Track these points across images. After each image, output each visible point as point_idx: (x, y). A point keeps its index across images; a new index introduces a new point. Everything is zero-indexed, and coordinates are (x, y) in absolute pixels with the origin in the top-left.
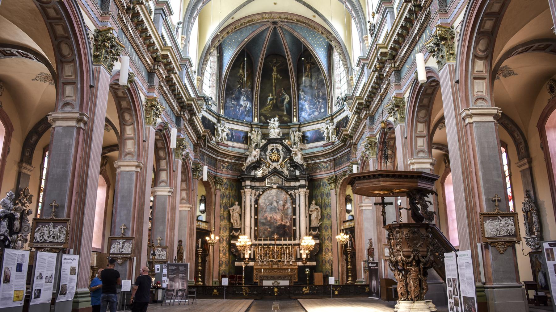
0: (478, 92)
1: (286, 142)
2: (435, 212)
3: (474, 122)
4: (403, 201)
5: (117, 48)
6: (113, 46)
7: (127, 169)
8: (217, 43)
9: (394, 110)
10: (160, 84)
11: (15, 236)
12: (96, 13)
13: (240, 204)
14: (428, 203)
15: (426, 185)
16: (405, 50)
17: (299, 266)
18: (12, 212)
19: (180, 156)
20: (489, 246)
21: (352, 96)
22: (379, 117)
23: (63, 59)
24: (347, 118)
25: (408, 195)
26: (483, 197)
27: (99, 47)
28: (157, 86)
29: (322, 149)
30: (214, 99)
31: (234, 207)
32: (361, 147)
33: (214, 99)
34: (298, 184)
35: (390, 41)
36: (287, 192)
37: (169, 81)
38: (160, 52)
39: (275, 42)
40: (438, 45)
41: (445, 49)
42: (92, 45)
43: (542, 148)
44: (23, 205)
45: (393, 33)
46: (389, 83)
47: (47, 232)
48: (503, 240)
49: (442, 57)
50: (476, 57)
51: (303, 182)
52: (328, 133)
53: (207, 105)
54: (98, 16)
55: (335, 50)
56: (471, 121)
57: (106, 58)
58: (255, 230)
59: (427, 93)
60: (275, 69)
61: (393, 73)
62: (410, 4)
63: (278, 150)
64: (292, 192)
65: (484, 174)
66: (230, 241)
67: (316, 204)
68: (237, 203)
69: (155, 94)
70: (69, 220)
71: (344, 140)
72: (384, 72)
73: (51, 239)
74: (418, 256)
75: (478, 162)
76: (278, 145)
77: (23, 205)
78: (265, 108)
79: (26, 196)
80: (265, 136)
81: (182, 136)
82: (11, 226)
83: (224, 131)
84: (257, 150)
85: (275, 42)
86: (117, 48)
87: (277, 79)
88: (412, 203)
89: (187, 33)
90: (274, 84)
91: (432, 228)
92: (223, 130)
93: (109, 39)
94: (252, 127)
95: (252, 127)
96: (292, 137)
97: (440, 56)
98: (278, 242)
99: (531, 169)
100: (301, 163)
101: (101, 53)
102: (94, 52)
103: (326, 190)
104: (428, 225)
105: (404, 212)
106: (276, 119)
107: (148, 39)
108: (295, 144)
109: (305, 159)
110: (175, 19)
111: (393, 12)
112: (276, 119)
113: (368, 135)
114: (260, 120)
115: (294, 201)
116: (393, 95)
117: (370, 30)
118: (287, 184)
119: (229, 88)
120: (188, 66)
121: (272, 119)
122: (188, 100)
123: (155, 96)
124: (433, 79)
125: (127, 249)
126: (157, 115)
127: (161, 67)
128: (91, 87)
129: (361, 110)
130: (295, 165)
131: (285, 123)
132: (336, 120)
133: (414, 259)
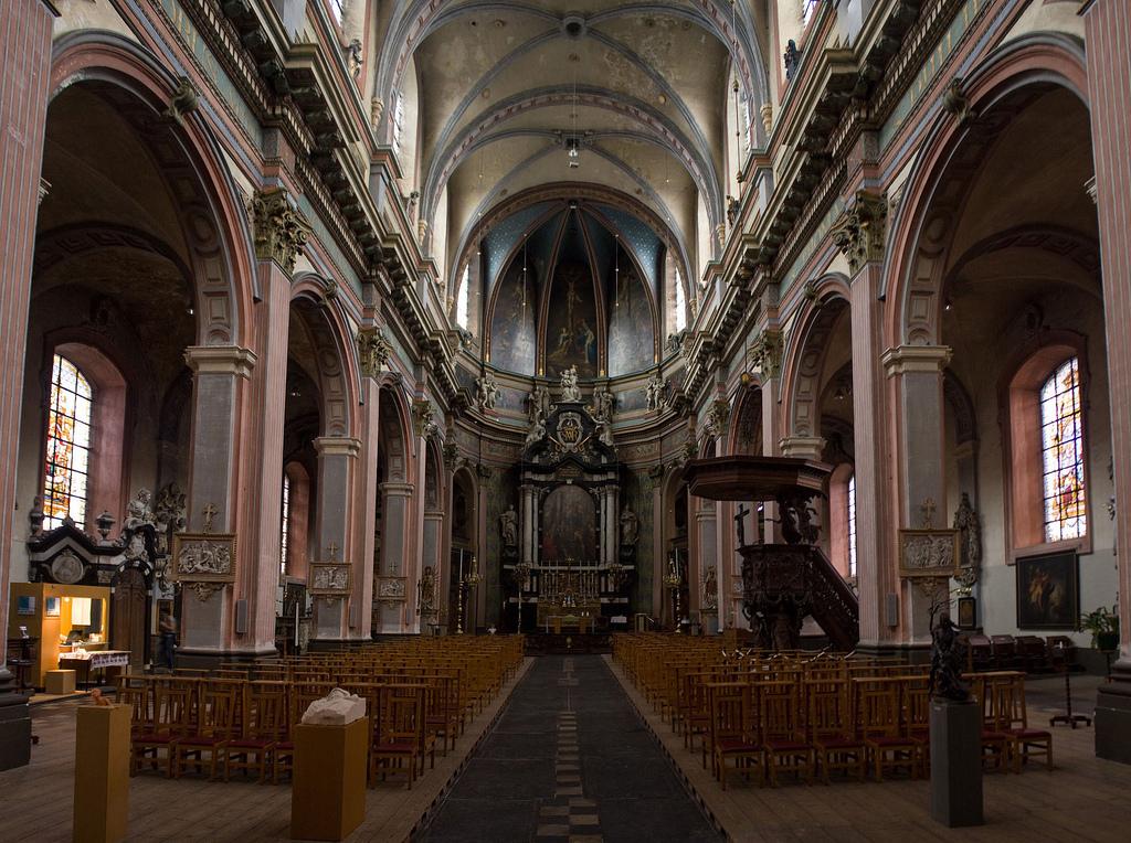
0: (916, 317)
1: (589, 410)
2: (820, 527)
3: (905, 371)
4: (769, 508)
5: (298, 229)
6: (290, 225)
7: (335, 451)
8: (479, 238)
9: (763, 354)
10: (383, 304)
11: (160, 562)
12: (255, 160)
13: (516, 509)
14: (811, 513)
15: (809, 482)
16: (792, 245)
17: (602, 604)
18: (149, 522)
19: (423, 431)
20: (909, 584)
21: (694, 333)
22: (739, 366)
23: (203, 249)
24: (683, 369)
25: (779, 499)
26: (907, 503)
27: (264, 225)
28: (378, 308)
29: (643, 421)
30: (475, 335)
31: (507, 513)
32: (705, 417)
33: (475, 335)
34: (604, 478)
35: (764, 228)
36: (588, 491)
37: (397, 297)
38: (382, 245)
39: (572, 232)
40: (854, 230)
41: (866, 238)
42: (251, 220)
43: (1000, 424)
44: (171, 510)
45: (722, 312)
46: (713, 381)
47: (199, 556)
48: (932, 574)
49: (861, 252)
50: (921, 252)
51: (611, 476)
52: (653, 395)
53: (464, 344)
54: (361, 309)
55: (668, 253)
56: (901, 370)
57: (280, 247)
58: (539, 550)
59: (828, 314)
60: (571, 286)
61: (863, 135)
62: (806, 153)
63: (574, 422)
64: (596, 490)
65: (912, 464)
66: (502, 565)
67: (630, 510)
68: (512, 507)
69: (284, 180)
70: (233, 536)
71: (677, 408)
72: (751, 288)
73: (206, 568)
74: (790, 597)
75: (905, 442)
76: (576, 414)
77: (171, 510)
78: (555, 353)
79: (173, 496)
80: (555, 398)
81: (425, 398)
82: (149, 546)
83: (492, 391)
84: (543, 421)
85: (572, 232)
86: (298, 229)
87: (575, 303)
88: (783, 511)
89: (428, 215)
90: (570, 312)
91: (813, 552)
92: (490, 390)
93: (282, 210)
94: (534, 385)
95: (534, 385)
96: (597, 401)
97: (856, 250)
98: (572, 568)
99: (976, 456)
100: (609, 445)
101: (269, 237)
102: (257, 235)
103: (647, 487)
104: (808, 547)
105: (768, 527)
106: (573, 370)
107: (358, 218)
108: (600, 413)
109: (616, 437)
110: (409, 184)
111: (771, 176)
112: (573, 370)
113: (717, 398)
114: (547, 373)
115: (598, 507)
116: (764, 328)
117: (729, 212)
118: (587, 478)
119: (491, 311)
120: (432, 275)
121: (567, 371)
122: (431, 334)
123: (375, 324)
124: (839, 296)
125: (340, 583)
126: (383, 360)
127: (383, 273)
128: (256, 300)
129: (707, 354)
130: (602, 449)
131: (586, 382)
132: (666, 374)
133: (783, 601)
